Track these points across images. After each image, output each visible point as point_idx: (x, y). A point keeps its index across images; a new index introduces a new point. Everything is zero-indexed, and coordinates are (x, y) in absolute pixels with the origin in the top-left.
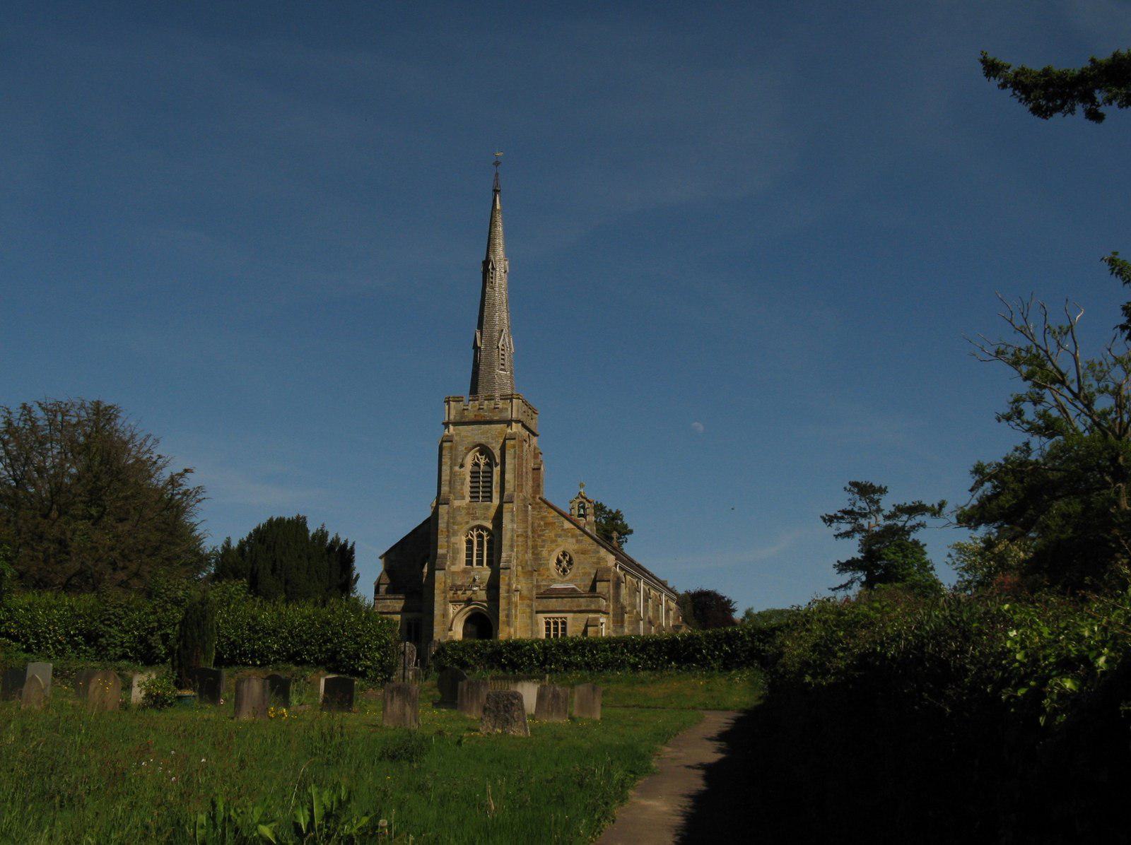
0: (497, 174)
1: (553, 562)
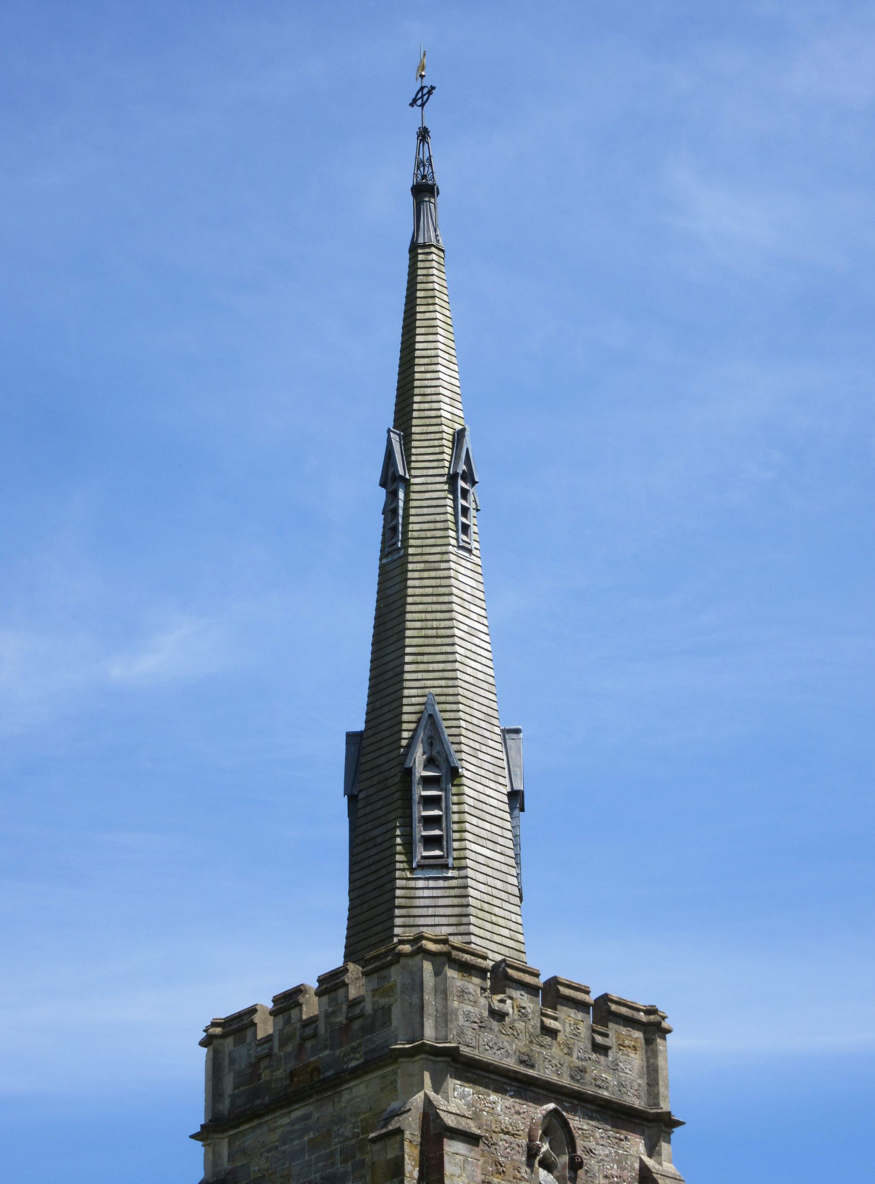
0: (423, 135)
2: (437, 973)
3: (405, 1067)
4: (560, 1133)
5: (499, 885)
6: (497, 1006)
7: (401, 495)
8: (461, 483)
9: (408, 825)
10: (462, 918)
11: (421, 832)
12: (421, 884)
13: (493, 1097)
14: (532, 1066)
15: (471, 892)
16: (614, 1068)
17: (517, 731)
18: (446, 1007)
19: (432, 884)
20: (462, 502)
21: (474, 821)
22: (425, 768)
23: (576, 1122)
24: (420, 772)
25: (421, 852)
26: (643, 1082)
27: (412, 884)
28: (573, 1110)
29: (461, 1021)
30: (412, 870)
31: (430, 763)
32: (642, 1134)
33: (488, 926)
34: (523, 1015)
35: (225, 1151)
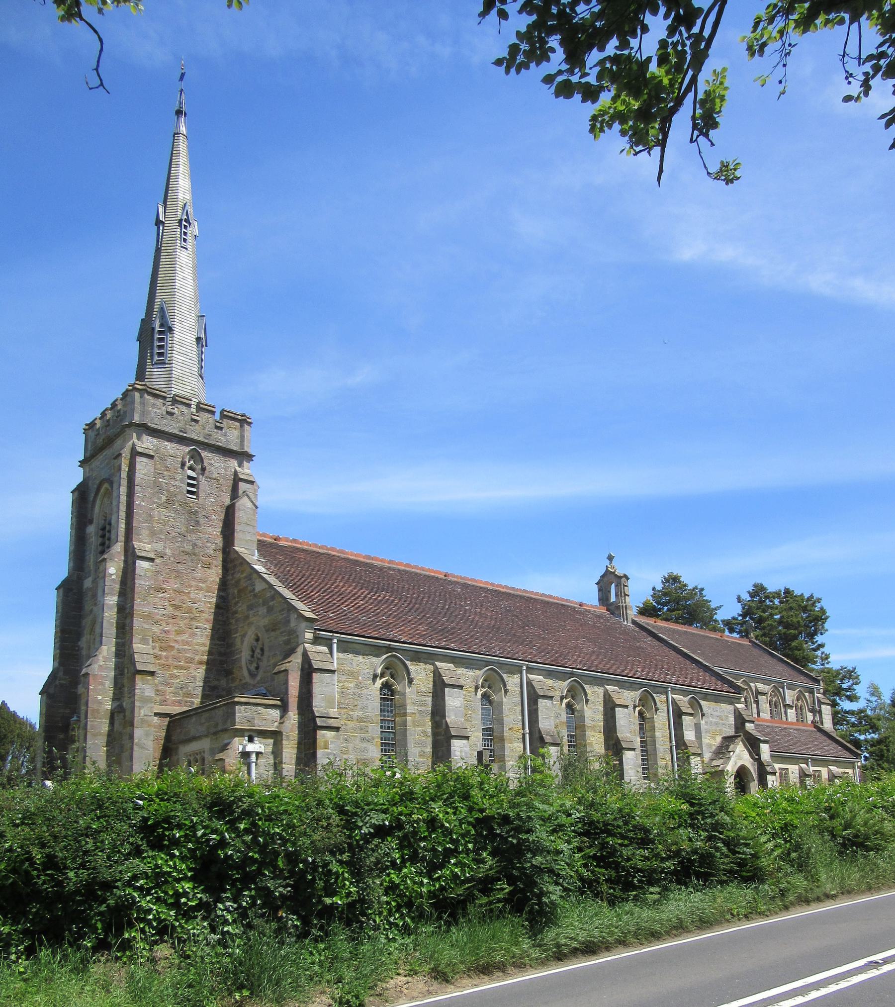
1: (245, 655)
2: (142, 396)
3: (128, 431)
4: (198, 457)
5: (188, 370)
6: (169, 410)
7: (161, 228)
8: (184, 223)
9: (152, 349)
10: (169, 382)
11: (156, 351)
12: (155, 370)
13: (166, 443)
14: (186, 433)
15: (174, 372)
16: (225, 435)
17: (203, 316)
18: (144, 409)
19: (159, 370)
20: (183, 230)
21: (178, 347)
22: (160, 327)
23: (204, 454)
24: (157, 329)
25: (156, 358)
26: (238, 441)
27: (152, 370)
28: (204, 449)
29: (152, 415)
30: (153, 365)
31: (162, 325)
32: (236, 459)
33: (181, 385)
34: (182, 413)
35: (87, 470)
